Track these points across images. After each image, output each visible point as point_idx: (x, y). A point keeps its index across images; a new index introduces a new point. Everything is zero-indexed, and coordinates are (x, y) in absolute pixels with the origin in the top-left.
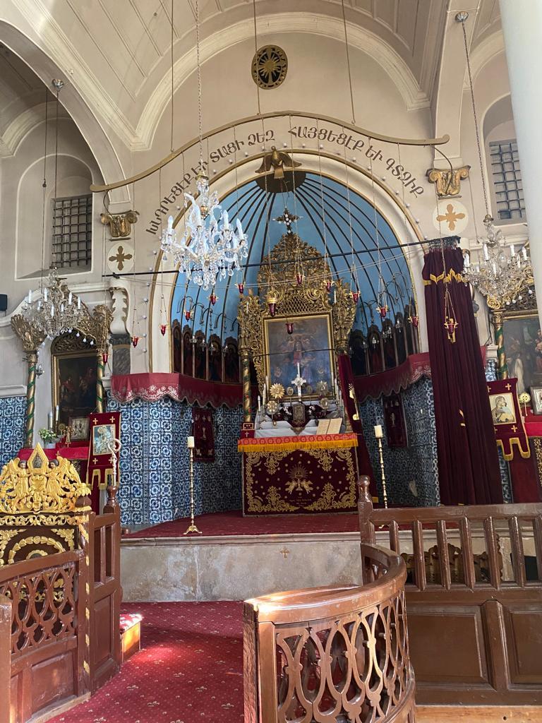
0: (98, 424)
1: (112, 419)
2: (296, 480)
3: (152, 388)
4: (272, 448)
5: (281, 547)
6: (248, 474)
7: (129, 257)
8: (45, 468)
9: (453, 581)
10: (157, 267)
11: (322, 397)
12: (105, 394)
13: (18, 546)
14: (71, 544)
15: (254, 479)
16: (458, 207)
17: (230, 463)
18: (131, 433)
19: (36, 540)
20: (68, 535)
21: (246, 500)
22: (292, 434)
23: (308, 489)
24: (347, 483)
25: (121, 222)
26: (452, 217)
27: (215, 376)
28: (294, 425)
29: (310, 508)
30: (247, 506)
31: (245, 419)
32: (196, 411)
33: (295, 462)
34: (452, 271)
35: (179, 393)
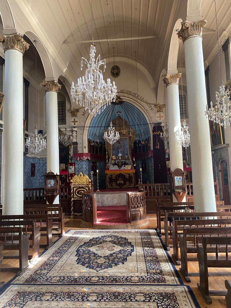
0: (70, 166)
1: (73, 164)
2: (120, 181)
3: (84, 157)
4: (114, 172)
5: (119, 194)
6: (108, 179)
7: (77, 122)
8: (82, 177)
9: (153, 195)
10: (85, 126)
11: (126, 159)
12: (71, 158)
13: (77, 190)
14: (88, 190)
15: (109, 180)
16: (162, 114)
17: (100, 176)
18: (78, 168)
19: (81, 189)
20: (87, 188)
21: (107, 185)
22: (118, 169)
23: (123, 183)
24: (132, 181)
25: (75, 112)
26: (160, 117)
27: (97, 153)
28: (119, 167)
29: (123, 187)
30: (107, 187)
31: (106, 165)
32: (93, 162)
33: (120, 176)
34: (159, 131)
35: (91, 158)
